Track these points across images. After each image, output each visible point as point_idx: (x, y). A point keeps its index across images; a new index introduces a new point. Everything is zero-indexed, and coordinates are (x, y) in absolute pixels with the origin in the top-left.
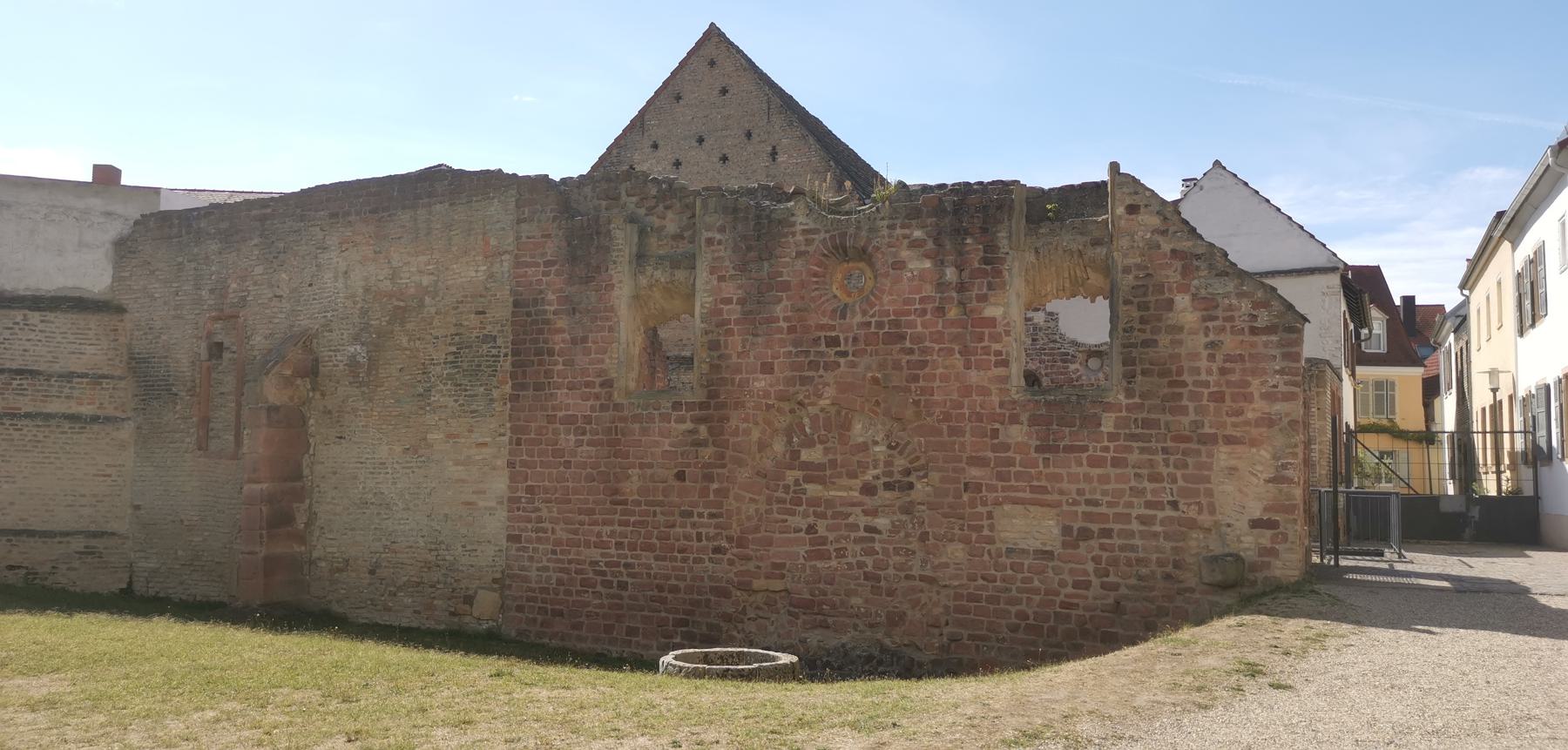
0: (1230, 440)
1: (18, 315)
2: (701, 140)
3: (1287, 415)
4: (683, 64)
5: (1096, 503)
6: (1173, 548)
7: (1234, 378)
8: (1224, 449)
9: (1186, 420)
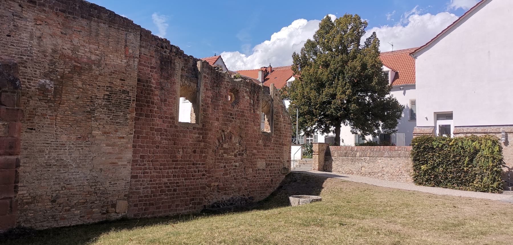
5: (270, 158)
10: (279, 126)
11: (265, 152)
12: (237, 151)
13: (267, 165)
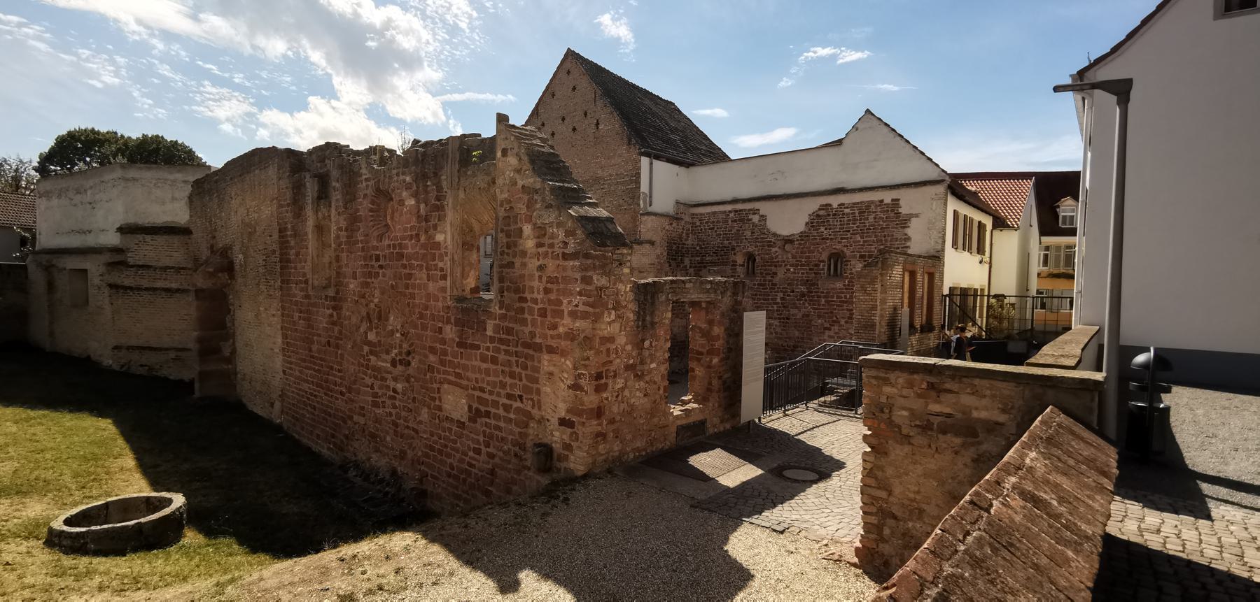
0: (551, 350)
1: (140, 237)
2: (563, 119)
3: (583, 331)
4: (555, 74)
5: (482, 390)
6: (520, 433)
7: (553, 296)
8: (546, 357)
9: (527, 330)
10: (517, 271)
11: (465, 368)
12: (395, 351)
13: (475, 415)
